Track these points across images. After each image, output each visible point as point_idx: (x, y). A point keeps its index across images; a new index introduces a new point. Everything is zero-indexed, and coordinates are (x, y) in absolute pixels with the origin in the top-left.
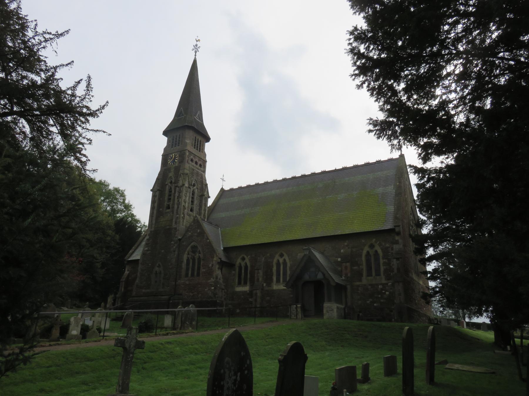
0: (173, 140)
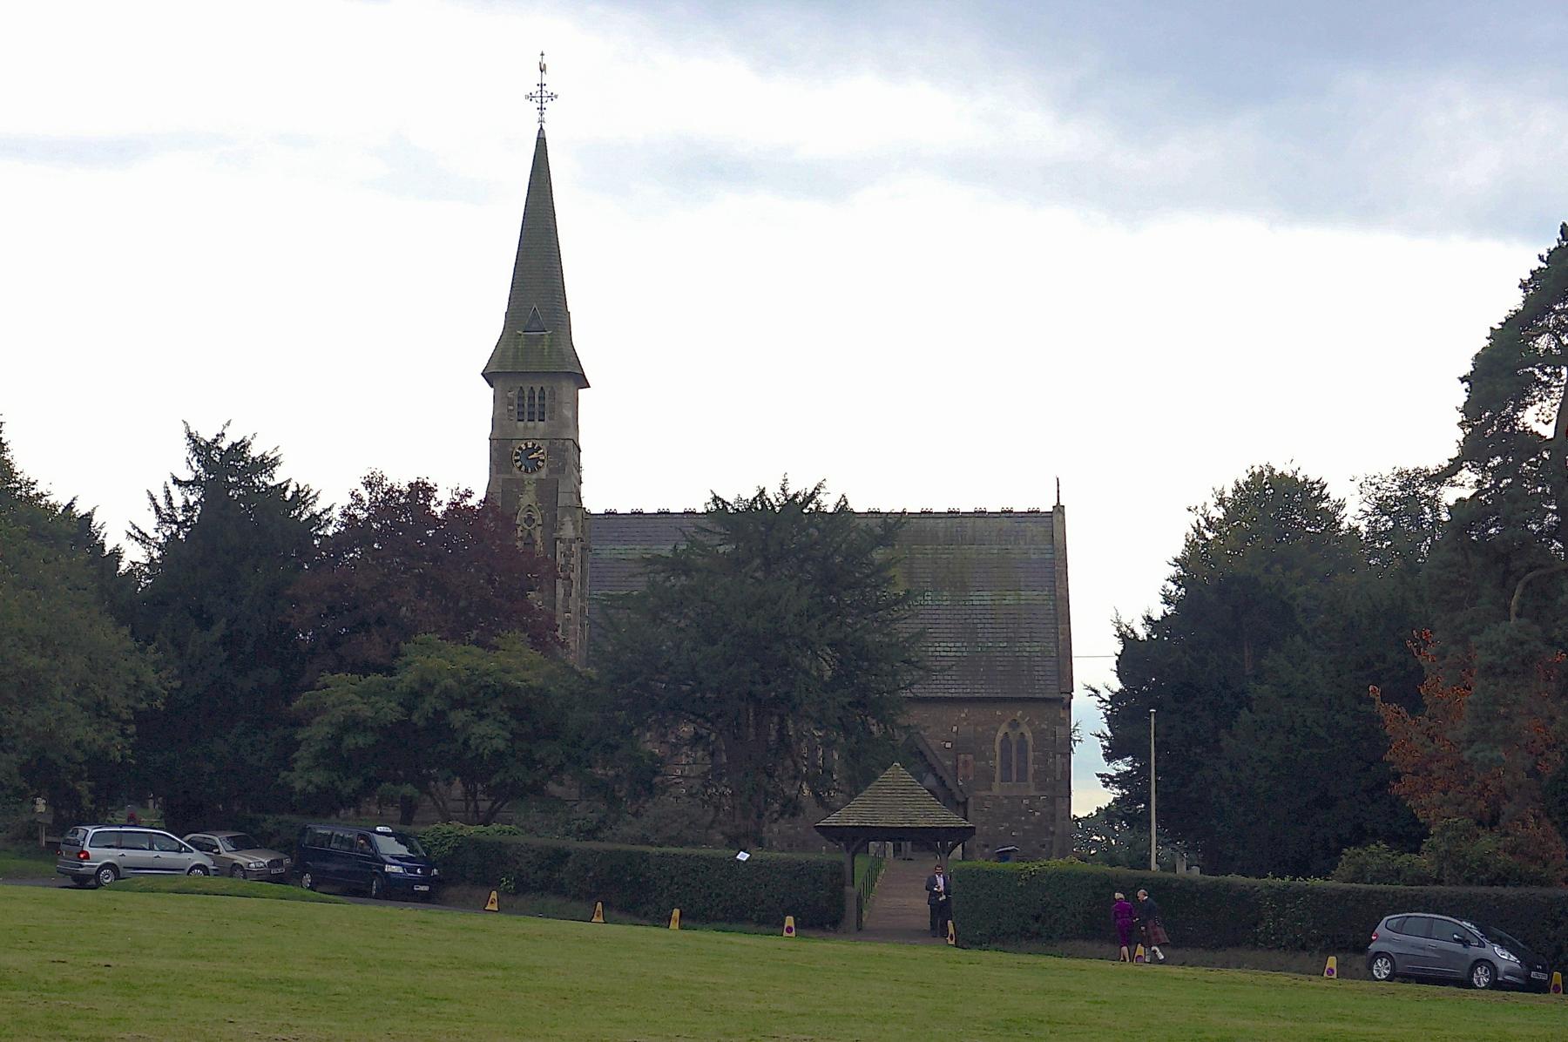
0: (521, 398)
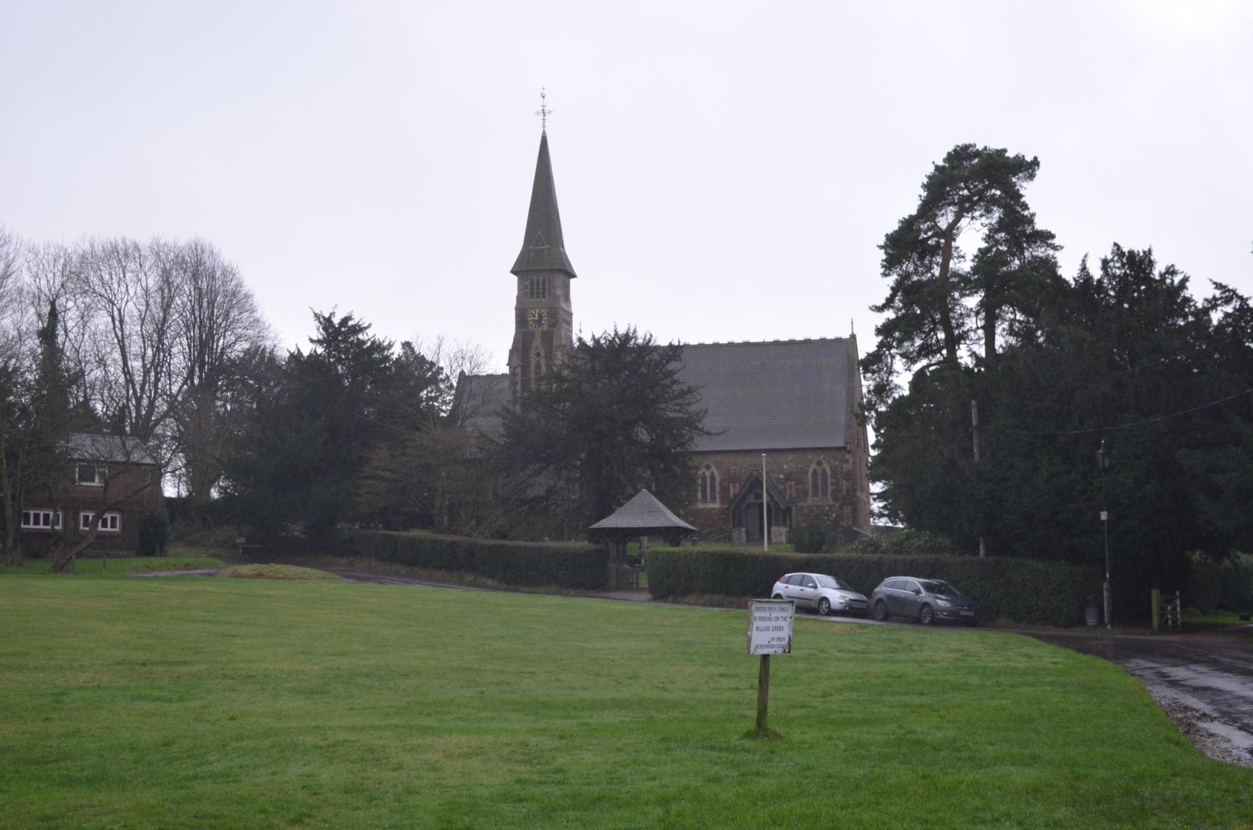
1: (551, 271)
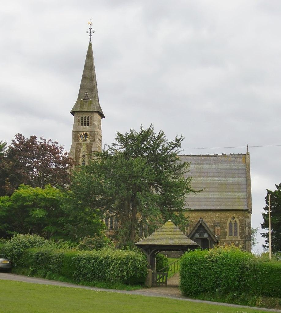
0: (82, 119)
1: (92, 112)
